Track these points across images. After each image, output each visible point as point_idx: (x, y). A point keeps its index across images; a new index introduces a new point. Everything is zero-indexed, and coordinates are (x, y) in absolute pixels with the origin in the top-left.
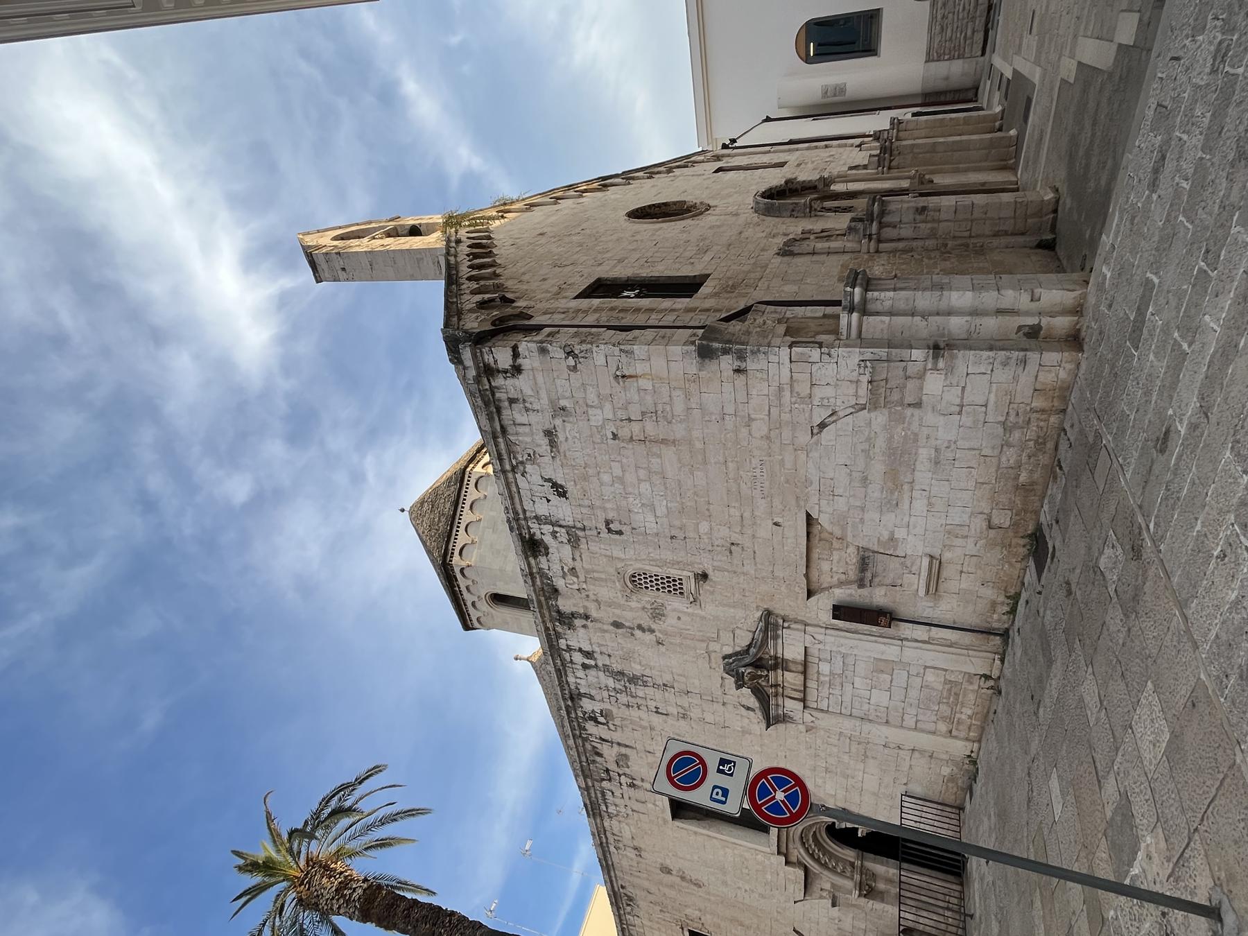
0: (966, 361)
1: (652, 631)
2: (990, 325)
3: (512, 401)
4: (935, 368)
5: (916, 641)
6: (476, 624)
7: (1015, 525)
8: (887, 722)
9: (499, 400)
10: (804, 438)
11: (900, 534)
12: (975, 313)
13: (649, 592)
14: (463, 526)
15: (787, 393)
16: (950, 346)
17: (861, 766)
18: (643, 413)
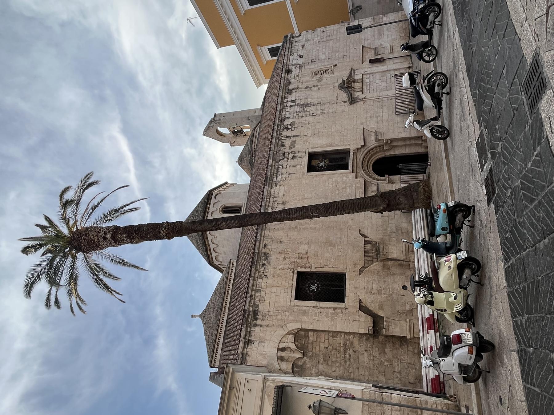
1: (317, 86)
5: (327, 308)
7: (405, 35)
11: (383, 43)
17: (381, 110)
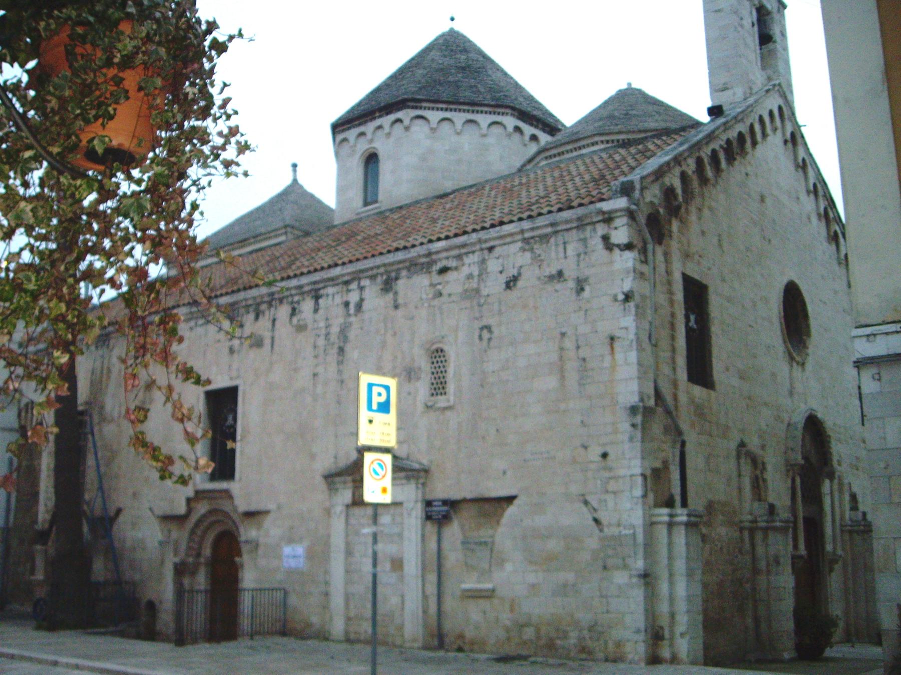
0: (638, 594)
2: (664, 608)
3: (584, 241)
4: (631, 576)
6: (340, 137)
8: (653, 524)
9: (584, 230)
10: (574, 489)
12: (672, 599)
13: (429, 365)
14: (448, 115)
15: (607, 474)
16: (647, 584)
18: (584, 360)
